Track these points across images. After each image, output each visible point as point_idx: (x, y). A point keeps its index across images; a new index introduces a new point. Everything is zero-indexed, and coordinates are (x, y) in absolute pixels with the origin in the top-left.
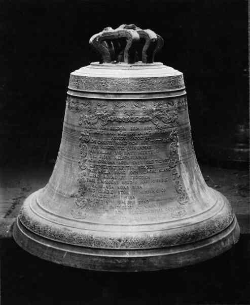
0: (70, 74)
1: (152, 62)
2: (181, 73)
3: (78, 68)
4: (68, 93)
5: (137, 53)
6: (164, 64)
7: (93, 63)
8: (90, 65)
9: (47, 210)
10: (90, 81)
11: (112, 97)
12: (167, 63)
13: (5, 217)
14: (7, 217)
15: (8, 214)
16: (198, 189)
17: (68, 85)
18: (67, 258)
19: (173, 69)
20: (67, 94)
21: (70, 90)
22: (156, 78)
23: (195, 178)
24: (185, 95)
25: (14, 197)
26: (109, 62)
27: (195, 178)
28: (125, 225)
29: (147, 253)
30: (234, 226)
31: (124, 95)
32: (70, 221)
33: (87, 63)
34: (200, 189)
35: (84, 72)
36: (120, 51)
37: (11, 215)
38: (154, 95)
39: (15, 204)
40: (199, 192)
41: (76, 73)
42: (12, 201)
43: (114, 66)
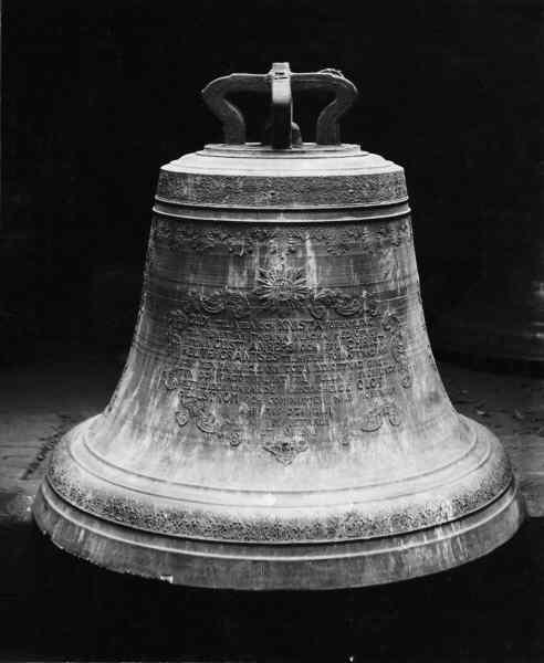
0: (151, 180)
2: (401, 169)
3: (176, 158)
6: (363, 149)
7: (207, 146)
10: (335, 183)
12: (369, 147)
13: (24, 478)
14: (30, 476)
15: (30, 472)
16: (126, 417)
18: (158, 563)
19: (383, 160)
21: (158, 202)
22: (216, 177)
23: (135, 393)
24: (406, 215)
27: (135, 393)
28: (214, 489)
29: (272, 554)
31: (299, 215)
33: (196, 146)
34: (129, 422)
36: (271, 129)
37: (36, 473)
39: (45, 450)
40: (122, 423)
42: (40, 444)
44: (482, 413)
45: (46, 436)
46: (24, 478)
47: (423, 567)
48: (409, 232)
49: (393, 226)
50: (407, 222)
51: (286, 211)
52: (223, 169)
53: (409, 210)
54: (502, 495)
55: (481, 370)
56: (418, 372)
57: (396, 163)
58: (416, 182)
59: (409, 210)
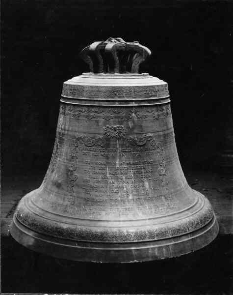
0: (61, 85)
1: (99, 72)
2: (166, 83)
4: (61, 100)
5: (121, 62)
6: (150, 75)
8: (81, 75)
9: (186, 209)
11: (117, 104)
13: (7, 217)
14: (9, 217)
17: (61, 93)
19: (158, 79)
20: (60, 101)
21: (63, 98)
25: (14, 199)
26: (106, 72)
30: (214, 223)
31: (83, 102)
32: (133, 223)
35: (75, 81)
36: (106, 63)
38: (96, 102)
41: (69, 82)
43: (107, 76)
44: (204, 189)
45: (16, 199)
46: (7, 217)
47: (152, 257)
48: (170, 111)
49: (164, 107)
50: (169, 105)
51: (118, 101)
52: (144, 83)
53: (170, 101)
54: (32, 230)
55: (198, 172)
56: (136, 172)
57: (164, 81)
58: (172, 90)
59: (170, 101)
